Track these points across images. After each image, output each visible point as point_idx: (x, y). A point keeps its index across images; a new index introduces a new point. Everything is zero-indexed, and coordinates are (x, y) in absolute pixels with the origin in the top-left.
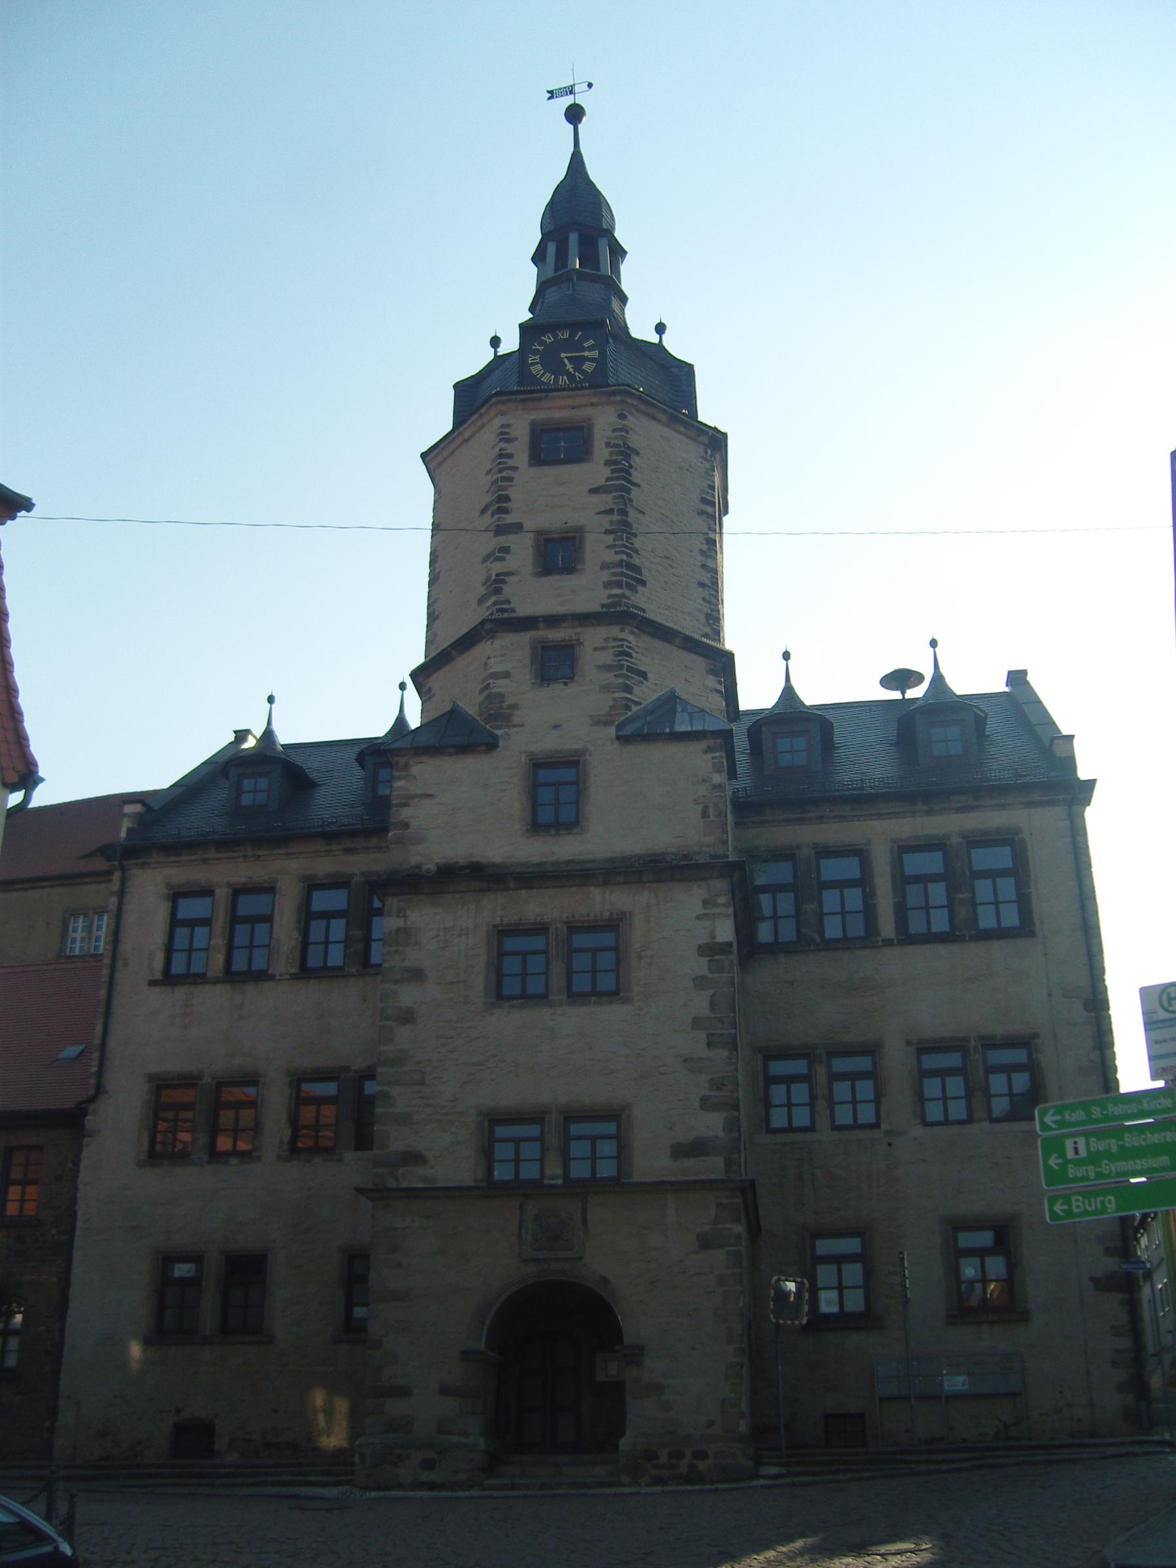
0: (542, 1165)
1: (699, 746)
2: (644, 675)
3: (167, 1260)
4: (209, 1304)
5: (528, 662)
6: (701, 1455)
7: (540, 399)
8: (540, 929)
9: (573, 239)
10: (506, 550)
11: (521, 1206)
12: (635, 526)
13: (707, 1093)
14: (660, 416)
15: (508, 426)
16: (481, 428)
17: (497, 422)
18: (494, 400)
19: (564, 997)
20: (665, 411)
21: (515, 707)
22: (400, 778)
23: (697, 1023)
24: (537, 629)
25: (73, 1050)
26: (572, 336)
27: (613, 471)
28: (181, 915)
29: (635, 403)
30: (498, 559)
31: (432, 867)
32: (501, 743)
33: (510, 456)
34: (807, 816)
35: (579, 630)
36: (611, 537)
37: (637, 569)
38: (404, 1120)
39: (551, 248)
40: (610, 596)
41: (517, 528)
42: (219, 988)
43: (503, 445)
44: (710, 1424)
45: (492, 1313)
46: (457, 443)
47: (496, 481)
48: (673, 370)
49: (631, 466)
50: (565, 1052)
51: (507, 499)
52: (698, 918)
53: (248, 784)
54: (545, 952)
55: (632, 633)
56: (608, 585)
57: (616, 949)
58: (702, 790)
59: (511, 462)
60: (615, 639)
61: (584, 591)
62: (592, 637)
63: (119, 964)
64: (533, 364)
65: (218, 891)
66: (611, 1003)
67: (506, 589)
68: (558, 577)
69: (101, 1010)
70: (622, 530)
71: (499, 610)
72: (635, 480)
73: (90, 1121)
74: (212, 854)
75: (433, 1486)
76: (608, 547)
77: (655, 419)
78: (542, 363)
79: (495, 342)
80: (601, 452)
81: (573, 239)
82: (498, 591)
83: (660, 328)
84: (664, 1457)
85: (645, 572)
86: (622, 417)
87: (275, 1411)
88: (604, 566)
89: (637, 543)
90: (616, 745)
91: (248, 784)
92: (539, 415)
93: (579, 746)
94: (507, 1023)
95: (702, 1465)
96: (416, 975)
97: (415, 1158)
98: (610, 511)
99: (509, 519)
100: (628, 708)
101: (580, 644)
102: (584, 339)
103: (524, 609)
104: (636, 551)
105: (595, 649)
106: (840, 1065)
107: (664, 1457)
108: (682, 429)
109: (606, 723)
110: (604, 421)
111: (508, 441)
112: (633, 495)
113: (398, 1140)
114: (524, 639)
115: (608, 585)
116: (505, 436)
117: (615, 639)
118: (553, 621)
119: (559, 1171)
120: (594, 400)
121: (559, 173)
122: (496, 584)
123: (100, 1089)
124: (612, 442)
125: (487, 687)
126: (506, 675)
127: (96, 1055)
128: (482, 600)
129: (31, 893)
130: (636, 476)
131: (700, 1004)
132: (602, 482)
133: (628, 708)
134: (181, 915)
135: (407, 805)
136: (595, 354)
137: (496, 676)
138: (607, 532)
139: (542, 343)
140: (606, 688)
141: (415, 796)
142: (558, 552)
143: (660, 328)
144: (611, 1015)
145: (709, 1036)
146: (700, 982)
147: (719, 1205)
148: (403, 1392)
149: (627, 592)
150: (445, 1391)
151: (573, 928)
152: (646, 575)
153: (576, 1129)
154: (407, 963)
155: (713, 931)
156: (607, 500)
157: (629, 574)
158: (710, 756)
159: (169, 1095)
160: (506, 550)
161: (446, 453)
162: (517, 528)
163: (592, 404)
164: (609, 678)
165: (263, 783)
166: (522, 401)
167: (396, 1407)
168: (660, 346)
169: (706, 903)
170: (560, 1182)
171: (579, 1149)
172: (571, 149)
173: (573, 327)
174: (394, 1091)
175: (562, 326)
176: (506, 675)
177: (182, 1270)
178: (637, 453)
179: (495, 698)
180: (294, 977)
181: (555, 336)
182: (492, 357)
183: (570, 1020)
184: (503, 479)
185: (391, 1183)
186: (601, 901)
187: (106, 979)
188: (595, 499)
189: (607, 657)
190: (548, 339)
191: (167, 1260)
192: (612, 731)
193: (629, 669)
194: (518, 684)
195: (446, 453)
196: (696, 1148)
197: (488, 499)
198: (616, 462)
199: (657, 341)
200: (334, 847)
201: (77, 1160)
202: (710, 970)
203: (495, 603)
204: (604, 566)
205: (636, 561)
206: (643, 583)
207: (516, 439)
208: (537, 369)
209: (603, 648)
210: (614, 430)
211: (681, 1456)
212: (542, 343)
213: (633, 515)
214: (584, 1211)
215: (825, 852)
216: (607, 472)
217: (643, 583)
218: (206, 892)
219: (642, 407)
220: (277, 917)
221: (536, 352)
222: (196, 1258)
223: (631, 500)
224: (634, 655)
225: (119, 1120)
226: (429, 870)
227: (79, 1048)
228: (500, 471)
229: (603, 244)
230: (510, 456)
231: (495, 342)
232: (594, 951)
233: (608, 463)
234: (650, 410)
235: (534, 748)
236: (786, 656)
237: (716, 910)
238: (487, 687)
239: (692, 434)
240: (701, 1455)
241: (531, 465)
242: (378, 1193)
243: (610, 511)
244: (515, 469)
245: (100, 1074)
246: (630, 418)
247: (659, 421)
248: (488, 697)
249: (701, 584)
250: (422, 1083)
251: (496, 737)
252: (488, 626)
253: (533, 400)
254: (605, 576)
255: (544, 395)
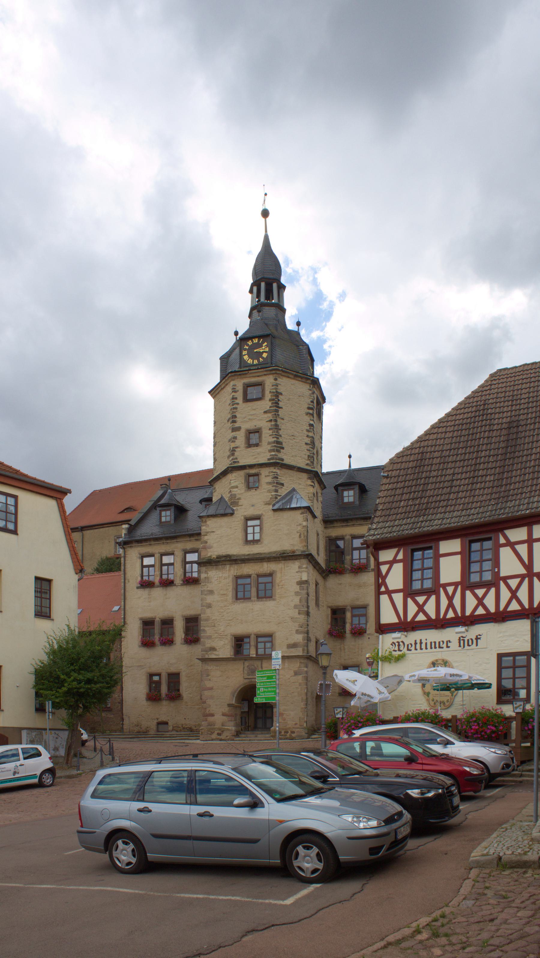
0: (300, 470)
1: (300, 512)
2: (282, 485)
3: (151, 675)
4: (164, 689)
5: (243, 481)
6: (293, 732)
7: (246, 374)
8: (249, 576)
9: (263, 285)
10: (235, 438)
11: (244, 663)
12: (280, 425)
13: (298, 628)
14: (290, 376)
15: (235, 385)
16: (227, 385)
17: (232, 383)
18: (230, 375)
19: (256, 599)
20: (292, 374)
21: (239, 499)
22: (204, 526)
23: (295, 607)
24: (246, 469)
25: (116, 608)
26: (259, 341)
27: (272, 403)
28: (145, 564)
29: (280, 373)
30: (233, 442)
31: (215, 556)
32: (235, 512)
33: (236, 398)
34: (349, 524)
35: (260, 469)
36: (271, 431)
37: (281, 443)
38: (210, 637)
39: (255, 289)
40: (271, 455)
41: (239, 429)
42: (159, 589)
43: (233, 394)
44: (296, 724)
45: (236, 694)
46: (220, 389)
47: (231, 409)
48: (300, 347)
49: (279, 400)
50: (253, 617)
51: (235, 417)
52: (297, 572)
53: (163, 513)
54: (250, 584)
55: (278, 469)
56: (270, 451)
57: (272, 583)
58: (299, 528)
59: (237, 401)
60: (272, 472)
61: (262, 454)
62: (265, 472)
63: (127, 581)
64: (245, 355)
65: (155, 555)
66: (270, 600)
67: (236, 454)
68: (253, 448)
69: (123, 597)
70: (276, 428)
71: (234, 462)
72: (280, 406)
73: (123, 634)
74: (153, 543)
75: (221, 740)
76: (270, 435)
77: (289, 377)
78: (248, 354)
79: (236, 333)
80: (268, 396)
81: (263, 285)
82: (233, 454)
83: (298, 324)
84: (283, 733)
85: (283, 444)
86: (276, 379)
87: (185, 719)
88: (269, 443)
89: (281, 432)
90: (272, 512)
91: (163, 513)
92: (247, 380)
93: (260, 513)
94: (240, 607)
95: (293, 735)
96: (211, 592)
97: (213, 649)
98: (271, 421)
99: (237, 425)
100: (276, 498)
101: (261, 474)
102: (263, 343)
103: (243, 462)
104: (280, 436)
105: (266, 476)
106: (356, 612)
107: (283, 733)
108: (300, 379)
109: (269, 504)
110: (269, 381)
111: (235, 392)
112: (279, 413)
113: (209, 643)
114: (242, 473)
115: (270, 451)
116: (234, 391)
117: (272, 472)
118: (251, 466)
119: (255, 652)
120: (265, 373)
121: (258, 248)
122: (233, 451)
123: (125, 623)
124: (272, 391)
125: (230, 492)
126: (237, 487)
127: (123, 612)
128: (229, 457)
129: (101, 529)
130: (281, 404)
131: (297, 600)
132: (268, 408)
133: (276, 498)
134: (145, 564)
135: (206, 535)
136: (267, 350)
137: (233, 487)
138: (270, 429)
139: (248, 345)
140: (269, 491)
141: (209, 532)
142: (253, 437)
143: (298, 324)
144: (269, 604)
145: (299, 610)
146: (297, 593)
147: (301, 662)
148: (212, 715)
149: (277, 453)
150: (224, 715)
151: (259, 576)
152: (284, 445)
153: (260, 639)
154: (208, 589)
155: (301, 576)
156: (270, 416)
157: (278, 446)
158: (302, 515)
159: (147, 624)
160: (235, 438)
161: (217, 392)
162: (239, 429)
163: (265, 375)
164: (270, 487)
165: (168, 513)
166: (240, 375)
167: (210, 719)
168: (298, 333)
169: (299, 567)
170: (255, 656)
171: (261, 645)
172: (263, 234)
173: (259, 337)
174: (206, 629)
175: (255, 337)
176: (237, 487)
177: (156, 678)
178: (281, 394)
179: (233, 496)
180: (182, 585)
181: (252, 341)
182: (234, 341)
183: (257, 606)
184: (234, 408)
185: (207, 657)
186: (266, 567)
187: (123, 586)
188: (266, 415)
189: (269, 479)
190: (250, 343)
191: (151, 675)
192: (271, 507)
193: (277, 483)
194: (240, 491)
195: (217, 392)
196: (294, 646)
197: (229, 416)
198: (273, 400)
199: (296, 330)
200: (192, 539)
201: (121, 646)
202: (300, 590)
203: (232, 459)
204: (269, 443)
205: (280, 440)
206: (283, 448)
207: (238, 391)
208: (246, 357)
209: (268, 476)
210: (273, 386)
211: (287, 732)
212: (248, 345)
213: (279, 421)
214: (262, 664)
215: (354, 537)
216: (270, 404)
217: (283, 448)
218: (152, 555)
219: (283, 374)
220: (175, 564)
221: (245, 350)
222: (159, 675)
223: (278, 415)
224: (279, 477)
225: (132, 635)
226: (214, 558)
227: (118, 607)
228: (233, 405)
229: (275, 285)
230: (236, 398)
231: (236, 333)
232: (265, 583)
233: (270, 400)
234: (286, 374)
235: (246, 514)
236: (350, 457)
237: (303, 570)
238: (230, 492)
239: (304, 380)
240: (293, 732)
241: (244, 402)
242: (204, 660)
243: (271, 421)
244: (238, 404)
245: (124, 618)
246: (278, 379)
247: (290, 378)
248: (231, 495)
249: (211, 592)
250: (214, 626)
251: (233, 510)
252: (230, 469)
253: (243, 374)
254: (269, 447)
255: (247, 372)
